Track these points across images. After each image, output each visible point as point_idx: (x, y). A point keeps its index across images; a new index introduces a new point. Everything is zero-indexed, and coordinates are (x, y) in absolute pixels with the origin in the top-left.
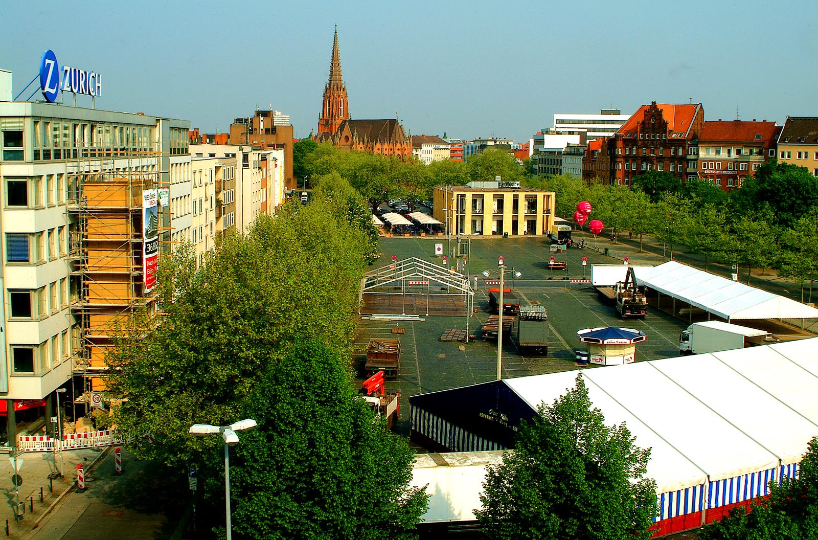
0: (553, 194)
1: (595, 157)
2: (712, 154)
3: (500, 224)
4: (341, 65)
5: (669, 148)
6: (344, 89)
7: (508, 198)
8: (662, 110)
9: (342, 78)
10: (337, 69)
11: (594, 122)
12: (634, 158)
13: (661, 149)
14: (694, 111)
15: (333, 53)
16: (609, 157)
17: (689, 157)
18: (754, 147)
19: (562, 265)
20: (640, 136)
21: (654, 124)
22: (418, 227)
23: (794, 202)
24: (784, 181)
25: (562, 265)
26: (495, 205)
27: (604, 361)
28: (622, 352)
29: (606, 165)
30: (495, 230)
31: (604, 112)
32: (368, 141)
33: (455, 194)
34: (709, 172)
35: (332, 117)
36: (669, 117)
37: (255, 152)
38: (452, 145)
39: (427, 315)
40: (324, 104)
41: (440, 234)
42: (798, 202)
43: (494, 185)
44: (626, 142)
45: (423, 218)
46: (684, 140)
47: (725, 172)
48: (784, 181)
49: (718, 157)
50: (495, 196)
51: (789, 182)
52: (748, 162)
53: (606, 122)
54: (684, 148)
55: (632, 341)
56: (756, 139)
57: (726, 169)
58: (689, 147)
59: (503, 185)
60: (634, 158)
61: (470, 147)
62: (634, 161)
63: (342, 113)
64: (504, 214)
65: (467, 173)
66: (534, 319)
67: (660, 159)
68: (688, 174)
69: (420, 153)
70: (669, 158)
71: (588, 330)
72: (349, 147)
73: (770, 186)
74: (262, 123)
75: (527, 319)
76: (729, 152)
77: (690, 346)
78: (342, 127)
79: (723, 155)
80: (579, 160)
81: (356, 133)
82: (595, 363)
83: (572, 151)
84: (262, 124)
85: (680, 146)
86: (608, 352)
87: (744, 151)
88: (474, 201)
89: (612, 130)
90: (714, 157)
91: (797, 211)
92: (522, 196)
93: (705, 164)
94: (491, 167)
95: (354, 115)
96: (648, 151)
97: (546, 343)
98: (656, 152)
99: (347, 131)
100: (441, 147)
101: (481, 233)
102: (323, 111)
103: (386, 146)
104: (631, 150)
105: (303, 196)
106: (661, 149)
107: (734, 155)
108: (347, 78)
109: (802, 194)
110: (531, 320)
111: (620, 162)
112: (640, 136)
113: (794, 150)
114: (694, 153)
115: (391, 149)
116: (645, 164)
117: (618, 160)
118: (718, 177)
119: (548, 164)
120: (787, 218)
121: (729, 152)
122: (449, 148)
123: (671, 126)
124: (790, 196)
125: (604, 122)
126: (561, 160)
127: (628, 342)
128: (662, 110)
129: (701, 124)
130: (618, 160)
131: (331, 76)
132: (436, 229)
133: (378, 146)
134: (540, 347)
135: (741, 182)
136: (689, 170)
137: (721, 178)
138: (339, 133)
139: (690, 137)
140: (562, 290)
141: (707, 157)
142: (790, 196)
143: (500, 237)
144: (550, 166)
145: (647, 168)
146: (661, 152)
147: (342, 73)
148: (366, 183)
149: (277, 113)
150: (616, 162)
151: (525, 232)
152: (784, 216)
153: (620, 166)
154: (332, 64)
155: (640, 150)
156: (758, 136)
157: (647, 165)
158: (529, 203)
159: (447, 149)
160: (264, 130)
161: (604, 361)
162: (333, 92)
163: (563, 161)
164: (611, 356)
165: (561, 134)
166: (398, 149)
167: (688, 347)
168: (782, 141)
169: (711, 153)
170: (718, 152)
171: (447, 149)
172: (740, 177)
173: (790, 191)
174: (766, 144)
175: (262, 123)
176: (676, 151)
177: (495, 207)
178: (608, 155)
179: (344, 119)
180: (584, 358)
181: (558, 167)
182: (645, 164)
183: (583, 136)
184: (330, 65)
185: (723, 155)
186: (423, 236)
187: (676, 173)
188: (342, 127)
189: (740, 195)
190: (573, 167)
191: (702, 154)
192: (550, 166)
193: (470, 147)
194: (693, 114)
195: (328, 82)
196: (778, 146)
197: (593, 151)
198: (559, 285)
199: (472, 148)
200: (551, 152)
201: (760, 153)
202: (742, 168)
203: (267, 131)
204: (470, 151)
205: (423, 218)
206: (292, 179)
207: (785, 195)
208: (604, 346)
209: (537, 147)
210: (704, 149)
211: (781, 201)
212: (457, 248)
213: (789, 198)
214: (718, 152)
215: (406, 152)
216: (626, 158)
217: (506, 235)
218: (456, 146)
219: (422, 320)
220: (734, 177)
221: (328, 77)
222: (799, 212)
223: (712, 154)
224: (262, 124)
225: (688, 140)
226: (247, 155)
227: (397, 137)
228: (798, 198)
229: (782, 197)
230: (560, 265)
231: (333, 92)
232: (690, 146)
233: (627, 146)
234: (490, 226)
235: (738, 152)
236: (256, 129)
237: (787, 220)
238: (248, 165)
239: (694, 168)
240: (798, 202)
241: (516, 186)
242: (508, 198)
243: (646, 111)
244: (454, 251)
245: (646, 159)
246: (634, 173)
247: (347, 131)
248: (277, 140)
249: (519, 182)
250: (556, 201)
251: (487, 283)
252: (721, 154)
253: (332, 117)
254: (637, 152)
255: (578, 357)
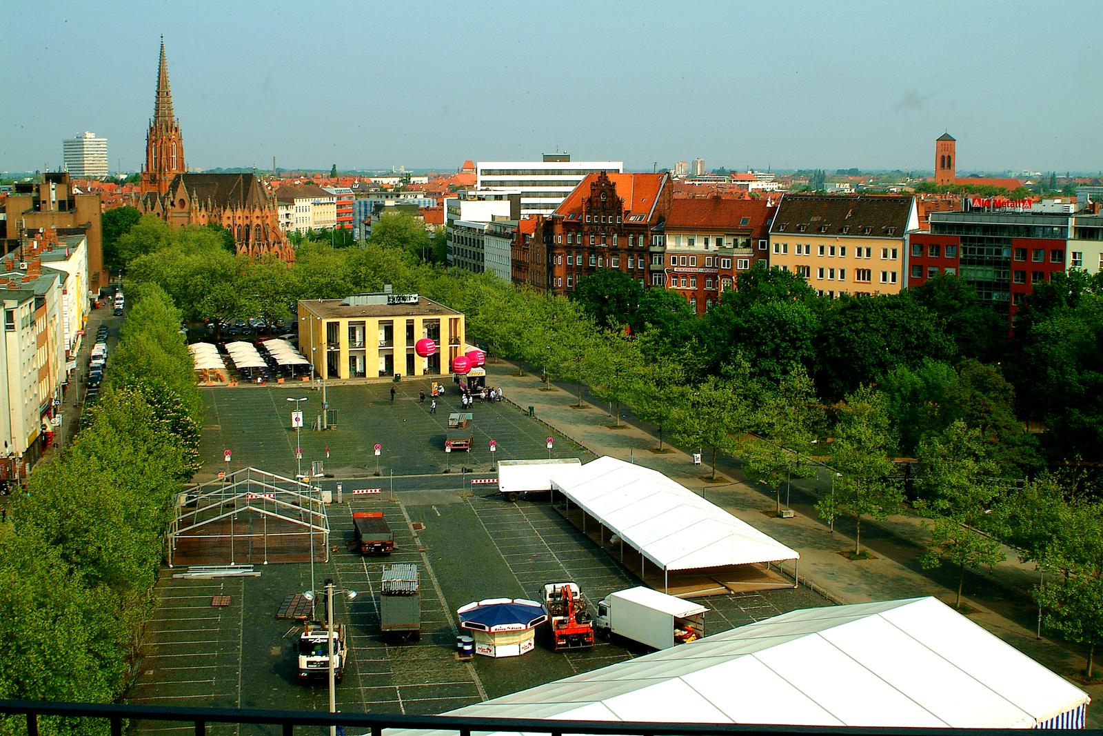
0: (462, 317)
1: (527, 242)
2: (684, 245)
3: (389, 360)
4: (171, 94)
5: (626, 236)
6: (176, 130)
7: (400, 325)
8: (614, 184)
9: (174, 112)
10: (166, 99)
11: (534, 172)
12: (579, 249)
13: (615, 236)
14: (660, 182)
15: (159, 77)
16: (545, 246)
17: (652, 249)
18: (739, 235)
19: (466, 445)
20: (586, 219)
21: (604, 203)
22: (274, 369)
23: (778, 345)
24: (766, 316)
25: (466, 445)
26: (381, 335)
27: (493, 652)
28: (517, 639)
29: (542, 257)
30: (383, 368)
31: (547, 158)
32: (213, 206)
33: (325, 322)
34: (680, 270)
35: (160, 170)
36: (624, 192)
37: (23, 305)
38: (339, 198)
39: (266, 563)
40: (147, 151)
41: (306, 379)
42: (784, 345)
43: (381, 300)
44: (568, 226)
45: (283, 351)
46: (645, 226)
47: (701, 270)
48: (766, 316)
49: (692, 248)
50: (380, 322)
51: (771, 318)
52: (732, 257)
53: (550, 172)
54: (646, 237)
55: (529, 625)
56: (741, 225)
57: (704, 267)
58: (652, 235)
59: (394, 299)
60: (579, 249)
61: (362, 203)
62: (578, 253)
63: (175, 163)
64: (395, 347)
65: (346, 276)
66: (400, 593)
67: (614, 251)
68: (651, 272)
69: (292, 211)
70: (626, 250)
71: (473, 605)
72: (185, 215)
73: (746, 322)
74: (53, 193)
75: (389, 593)
76: (706, 243)
77: (609, 623)
78: (175, 186)
79: (699, 245)
80: (506, 245)
81: (195, 195)
82: (482, 653)
83: (498, 230)
84: (53, 194)
85: (640, 234)
86: (498, 640)
87: (727, 242)
88: (352, 331)
89: (552, 206)
90: (688, 249)
91: (783, 358)
92: (418, 322)
93: (674, 259)
94: (380, 266)
95: (196, 165)
96: (597, 240)
97: (417, 626)
98: (609, 241)
99: (182, 192)
100: (322, 202)
101: (363, 374)
102: (147, 161)
103: (239, 213)
104: (574, 237)
105: (117, 299)
106: (615, 236)
107: (713, 246)
108: (180, 111)
109: (788, 335)
110: (395, 595)
111: (561, 254)
112: (586, 219)
113: (793, 241)
114: (660, 243)
115: (247, 217)
116: (593, 257)
117: (557, 252)
118: (692, 277)
119: (470, 245)
120: (770, 368)
121: (706, 243)
122: (335, 201)
123: (627, 205)
124: (774, 337)
125: (547, 172)
126: (483, 241)
127: (523, 627)
128: (614, 184)
129: (669, 201)
130: (557, 252)
131: (157, 110)
132: (301, 371)
133: (228, 213)
134: (408, 632)
135: (724, 284)
136: (653, 267)
137: (696, 278)
138: (171, 195)
139: (654, 221)
140: (457, 496)
141: (677, 248)
142: (774, 337)
143: (389, 380)
144: (469, 248)
145: (596, 264)
146: (615, 240)
147: (173, 106)
148: (203, 296)
149: (89, 135)
150: (554, 254)
151: (425, 370)
152: (766, 364)
153: (559, 260)
154: (158, 93)
155: (586, 238)
156: (745, 221)
157: (596, 259)
158: (429, 330)
159: (331, 203)
160: (57, 203)
161: (493, 652)
162: (162, 132)
163: (485, 244)
164: (502, 645)
165: (484, 199)
166: (257, 217)
167: (607, 624)
168: (777, 229)
169: (682, 244)
170: (691, 242)
171: (331, 203)
172: (721, 277)
173: (773, 330)
174: (758, 231)
175: (53, 193)
176: (635, 240)
177: (383, 337)
178: (544, 243)
179: (178, 172)
180: (468, 648)
181: (479, 250)
182: (593, 257)
183: (515, 200)
184: (155, 94)
185: (699, 245)
186: (282, 383)
187: (635, 270)
188: (175, 186)
189: (711, 325)
190: (498, 256)
191: (671, 244)
192: (469, 248)
193: (362, 203)
194: (657, 189)
195: (153, 119)
196: (771, 237)
197: (524, 235)
198: (455, 483)
199: (366, 205)
200: (469, 228)
201: (747, 245)
202: (724, 266)
203: (62, 205)
204: (363, 209)
205: (283, 351)
206: (101, 273)
207: (766, 336)
208: (493, 635)
209: (453, 217)
210: (673, 238)
211: (760, 344)
212: (322, 417)
213: (772, 340)
214: (691, 242)
215: (268, 221)
216: (568, 249)
217: (398, 377)
218: (345, 199)
219: (258, 574)
220: (714, 276)
221: (153, 112)
222: (785, 358)
223: (684, 245)
224: (53, 194)
225: (653, 225)
226: (12, 312)
227: (256, 199)
228: (783, 340)
229: (762, 338)
230: (462, 445)
231: (162, 132)
232: (654, 233)
233: (569, 231)
234: (375, 365)
235: (719, 242)
236: (44, 202)
237: (770, 371)
238: (12, 327)
239: (660, 263)
240: (784, 345)
241: (413, 301)
242: (400, 325)
243: (593, 184)
244: (319, 421)
245: (593, 250)
246: (579, 268)
247: (182, 192)
248: (75, 218)
249: (416, 295)
250: (467, 325)
251: (356, 492)
252: (696, 244)
253: (160, 170)
254: (583, 241)
255: (460, 645)
